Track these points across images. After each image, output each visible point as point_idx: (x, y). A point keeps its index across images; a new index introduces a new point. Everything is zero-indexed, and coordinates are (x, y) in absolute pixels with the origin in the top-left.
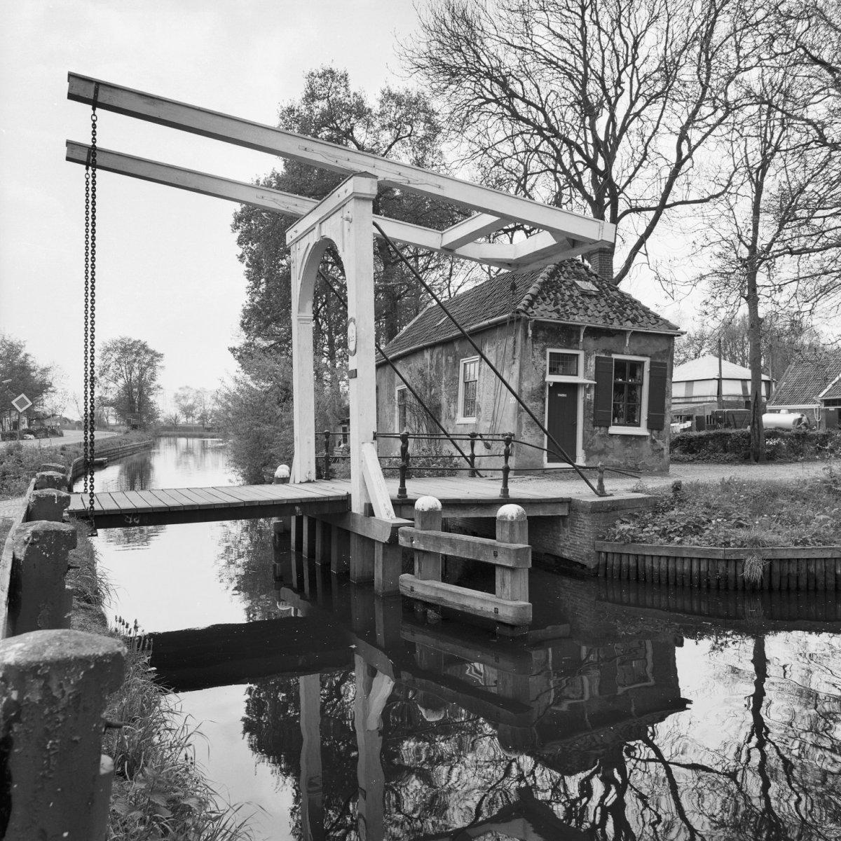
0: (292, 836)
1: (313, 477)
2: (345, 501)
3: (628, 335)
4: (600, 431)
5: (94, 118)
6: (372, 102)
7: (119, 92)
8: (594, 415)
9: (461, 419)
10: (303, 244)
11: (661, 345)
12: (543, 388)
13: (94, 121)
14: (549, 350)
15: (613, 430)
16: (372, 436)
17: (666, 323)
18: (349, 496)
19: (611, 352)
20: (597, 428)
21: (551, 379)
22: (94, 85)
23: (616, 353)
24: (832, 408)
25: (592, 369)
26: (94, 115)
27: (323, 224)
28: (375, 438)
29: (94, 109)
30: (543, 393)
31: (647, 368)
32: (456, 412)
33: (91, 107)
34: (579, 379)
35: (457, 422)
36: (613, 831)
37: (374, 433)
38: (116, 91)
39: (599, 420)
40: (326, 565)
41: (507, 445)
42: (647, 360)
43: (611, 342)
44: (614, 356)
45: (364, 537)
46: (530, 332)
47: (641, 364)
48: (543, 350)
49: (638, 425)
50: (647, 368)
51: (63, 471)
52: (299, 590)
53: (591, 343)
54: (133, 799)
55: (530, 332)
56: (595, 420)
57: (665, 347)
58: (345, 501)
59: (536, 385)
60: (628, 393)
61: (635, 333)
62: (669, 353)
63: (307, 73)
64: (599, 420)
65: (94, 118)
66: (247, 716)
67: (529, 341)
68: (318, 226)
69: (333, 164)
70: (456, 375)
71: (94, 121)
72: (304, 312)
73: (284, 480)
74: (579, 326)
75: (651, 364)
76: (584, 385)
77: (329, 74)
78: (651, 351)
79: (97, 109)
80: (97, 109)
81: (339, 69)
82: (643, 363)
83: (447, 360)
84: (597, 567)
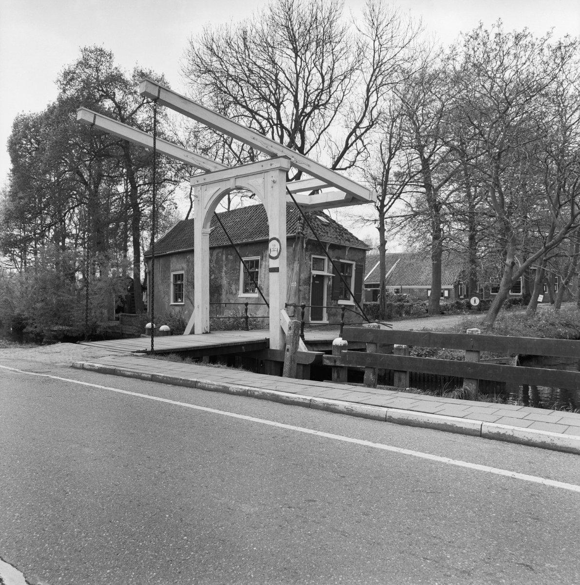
3: (347, 249)
4: (333, 302)
6: (128, 77)
7: (170, 94)
8: (332, 294)
9: (241, 294)
11: (360, 255)
12: (310, 278)
14: (313, 256)
15: (341, 302)
16: (285, 305)
17: (362, 242)
19: (339, 258)
20: (333, 301)
21: (315, 273)
23: (342, 259)
24: (369, 289)
25: (331, 267)
28: (286, 307)
30: (310, 280)
31: (354, 268)
32: (238, 290)
34: (325, 273)
35: (239, 296)
37: (286, 304)
38: (168, 93)
39: (334, 297)
41: (303, 309)
42: (354, 263)
43: (338, 252)
44: (341, 261)
46: (305, 245)
47: (351, 265)
48: (310, 256)
50: (354, 268)
53: (331, 253)
54: (275, 516)
55: (305, 245)
56: (332, 296)
57: (362, 256)
58: (266, 342)
59: (307, 276)
60: (345, 280)
61: (351, 248)
62: (364, 259)
63: (82, 48)
64: (334, 297)
67: (304, 250)
69: (265, 148)
70: (237, 267)
72: (206, 228)
74: (326, 243)
75: (356, 265)
76: (328, 276)
77: (101, 52)
78: (356, 258)
81: (107, 49)
82: (352, 264)
83: (227, 258)
84: (385, 375)
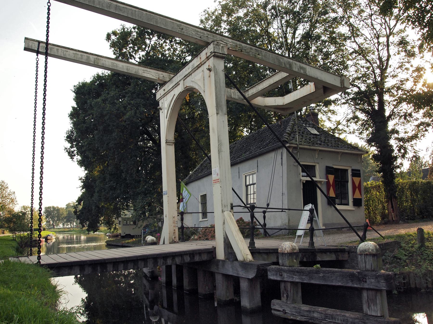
0: (69, 119)
1: (177, 239)
2: (212, 252)
5: (37, 59)
10: (169, 97)
13: (37, 61)
18: (215, 248)
22: (37, 43)
26: (37, 58)
27: (185, 81)
29: (37, 55)
33: (36, 54)
36: (176, 299)
40: (180, 286)
45: (227, 275)
49: (347, 204)
51: (412, 267)
52: (170, 308)
58: (212, 252)
65: (37, 59)
66: (76, 106)
68: (182, 81)
71: (37, 61)
73: (153, 243)
79: (39, 55)
80: (39, 55)
